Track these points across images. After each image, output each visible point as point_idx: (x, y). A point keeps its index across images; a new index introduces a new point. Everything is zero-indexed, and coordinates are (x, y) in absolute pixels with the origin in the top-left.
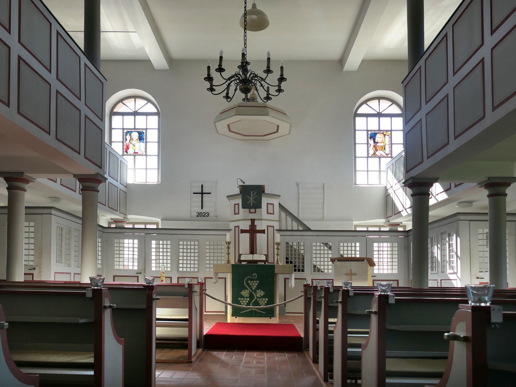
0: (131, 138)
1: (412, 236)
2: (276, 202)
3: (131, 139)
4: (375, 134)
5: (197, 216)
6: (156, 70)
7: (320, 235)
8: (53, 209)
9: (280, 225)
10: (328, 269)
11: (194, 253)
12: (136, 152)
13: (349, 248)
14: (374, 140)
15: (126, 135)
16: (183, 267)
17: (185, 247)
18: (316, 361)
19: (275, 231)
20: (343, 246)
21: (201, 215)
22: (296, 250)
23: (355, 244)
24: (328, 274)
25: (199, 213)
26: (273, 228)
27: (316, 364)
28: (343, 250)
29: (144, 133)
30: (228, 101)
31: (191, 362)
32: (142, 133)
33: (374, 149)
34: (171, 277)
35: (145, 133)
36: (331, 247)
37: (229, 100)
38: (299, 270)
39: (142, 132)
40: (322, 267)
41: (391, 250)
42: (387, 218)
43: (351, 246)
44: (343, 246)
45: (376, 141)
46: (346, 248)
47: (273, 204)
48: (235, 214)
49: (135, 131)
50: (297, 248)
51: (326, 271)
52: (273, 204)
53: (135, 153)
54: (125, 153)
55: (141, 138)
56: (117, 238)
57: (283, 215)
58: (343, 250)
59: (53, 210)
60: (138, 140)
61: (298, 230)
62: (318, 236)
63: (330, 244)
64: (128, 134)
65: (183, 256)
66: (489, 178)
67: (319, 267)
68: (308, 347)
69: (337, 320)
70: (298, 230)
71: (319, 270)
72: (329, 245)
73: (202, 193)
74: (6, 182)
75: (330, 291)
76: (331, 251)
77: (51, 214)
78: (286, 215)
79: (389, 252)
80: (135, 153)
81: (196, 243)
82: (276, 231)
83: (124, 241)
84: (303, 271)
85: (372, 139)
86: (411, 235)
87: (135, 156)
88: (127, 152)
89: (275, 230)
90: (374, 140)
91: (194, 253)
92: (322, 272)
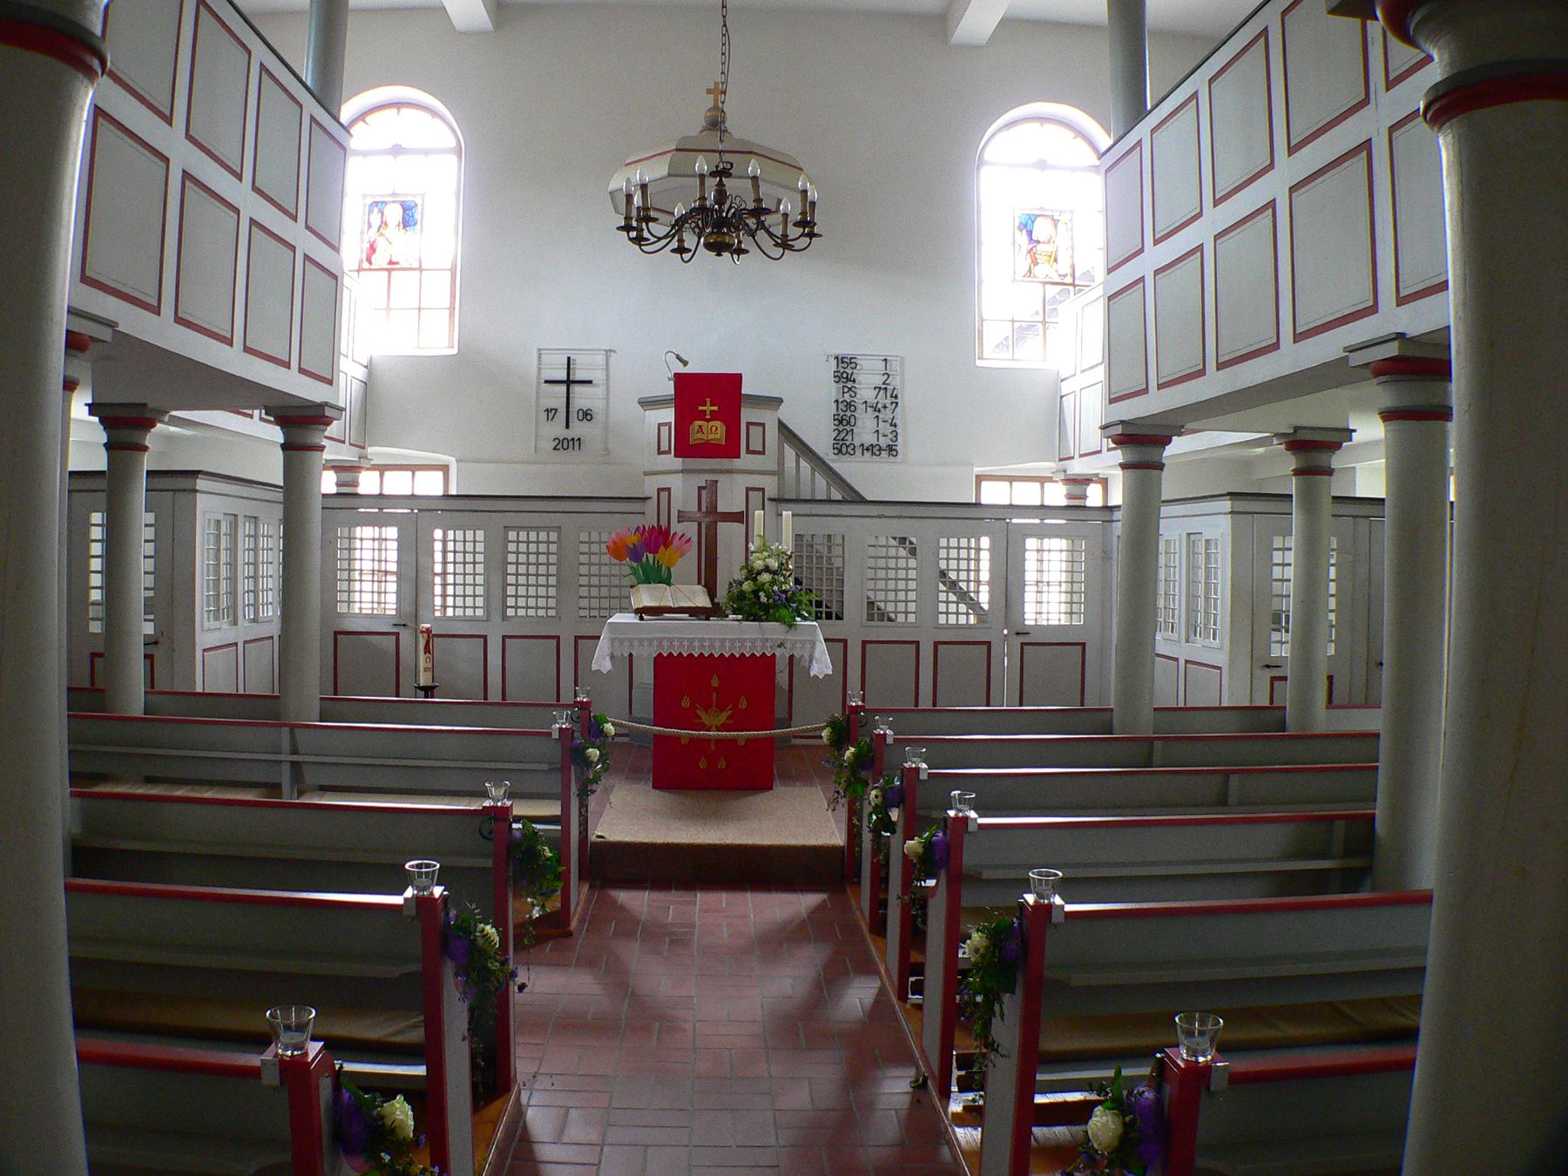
0: (382, 222)
1: (1120, 523)
2: (768, 417)
3: (384, 224)
4: (1033, 218)
5: (555, 449)
6: (460, 33)
7: (886, 515)
8: (200, 476)
9: (781, 485)
10: (906, 613)
11: (548, 564)
12: (394, 260)
13: (963, 554)
14: (1030, 233)
15: (370, 211)
16: (516, 607)
17: (523, 547)
18: (879, 927)
19: (766, 502)
20: (948, 548)
21: (565, 447)
22: (822, 557)
23: (978, 541)
24: (906, 625)
25: (561, 439)
26: (751, 449)
27: (878, 939)
28: (948, 559)
29: (416, 205)
30: (686, 260)
31: (570, 934)
32: (413, 208)
33: (1029, 260)
34: (486, 636)
35: (419, 207)
36: (915, 549)
37: (687, 256)
38: (829, 616)
39: (413, 204)
40: (890, 607)
41: (1070, 580)
42: (1061, 460)
43: (969, 548)
44: (948, 548)
45: (1034, 238)
46: (953, 553)
47: (763, 425)
48: (660, 452)
49: (394, 202)
50: (826, 553)
51: (901, 618)
52: (763, 425)
53: (391, 263)
54: (366, 265)
55: (407, 222)
56: (342, 525)
57: (790, 452)
58: (948, 559)
59: (202, 479)
60: (402, 226)
61: (830, 501)
62: (880, 517)
63: (914, 540)
64: (376, 210)
65: (517, 575)
66: (1297, 429)
67: (882, 605)
68: (859, 875)
69: (937, 883)
70: (830, 501)
71: (883, 616)
72: (911, 543)
73: (569, 382)
74: (102, 427)
75: (921, 778)
76: (916, 559)
77: (197, 491)
78: (797, 454)
79: (1064, 585)
80: (391, 263)
81: (553, 536)
82: (770, 502)
83: (393, 582)
84: (839, 618)
85: (1024, 231)
86: (1119, 521)
87: (389, 271)
88: (369, 261)
89: (769, 499)
90: (1030, 233)
91: (548, 564)
92: (890, 620)
